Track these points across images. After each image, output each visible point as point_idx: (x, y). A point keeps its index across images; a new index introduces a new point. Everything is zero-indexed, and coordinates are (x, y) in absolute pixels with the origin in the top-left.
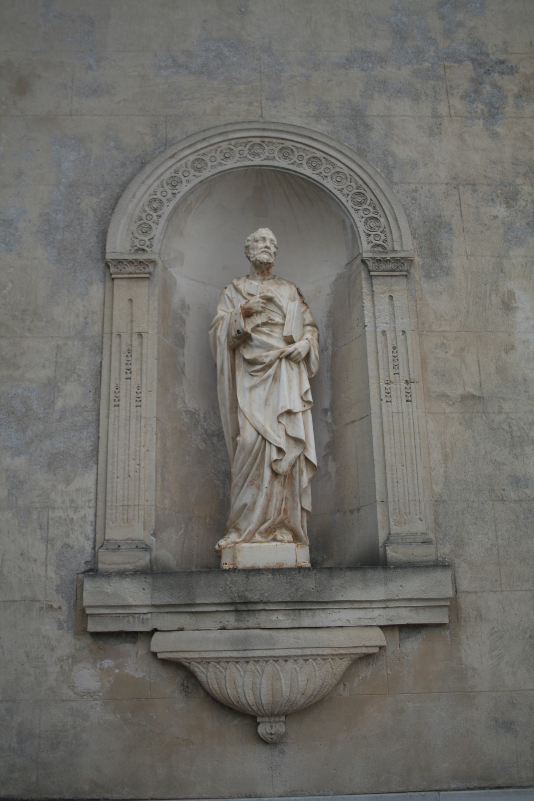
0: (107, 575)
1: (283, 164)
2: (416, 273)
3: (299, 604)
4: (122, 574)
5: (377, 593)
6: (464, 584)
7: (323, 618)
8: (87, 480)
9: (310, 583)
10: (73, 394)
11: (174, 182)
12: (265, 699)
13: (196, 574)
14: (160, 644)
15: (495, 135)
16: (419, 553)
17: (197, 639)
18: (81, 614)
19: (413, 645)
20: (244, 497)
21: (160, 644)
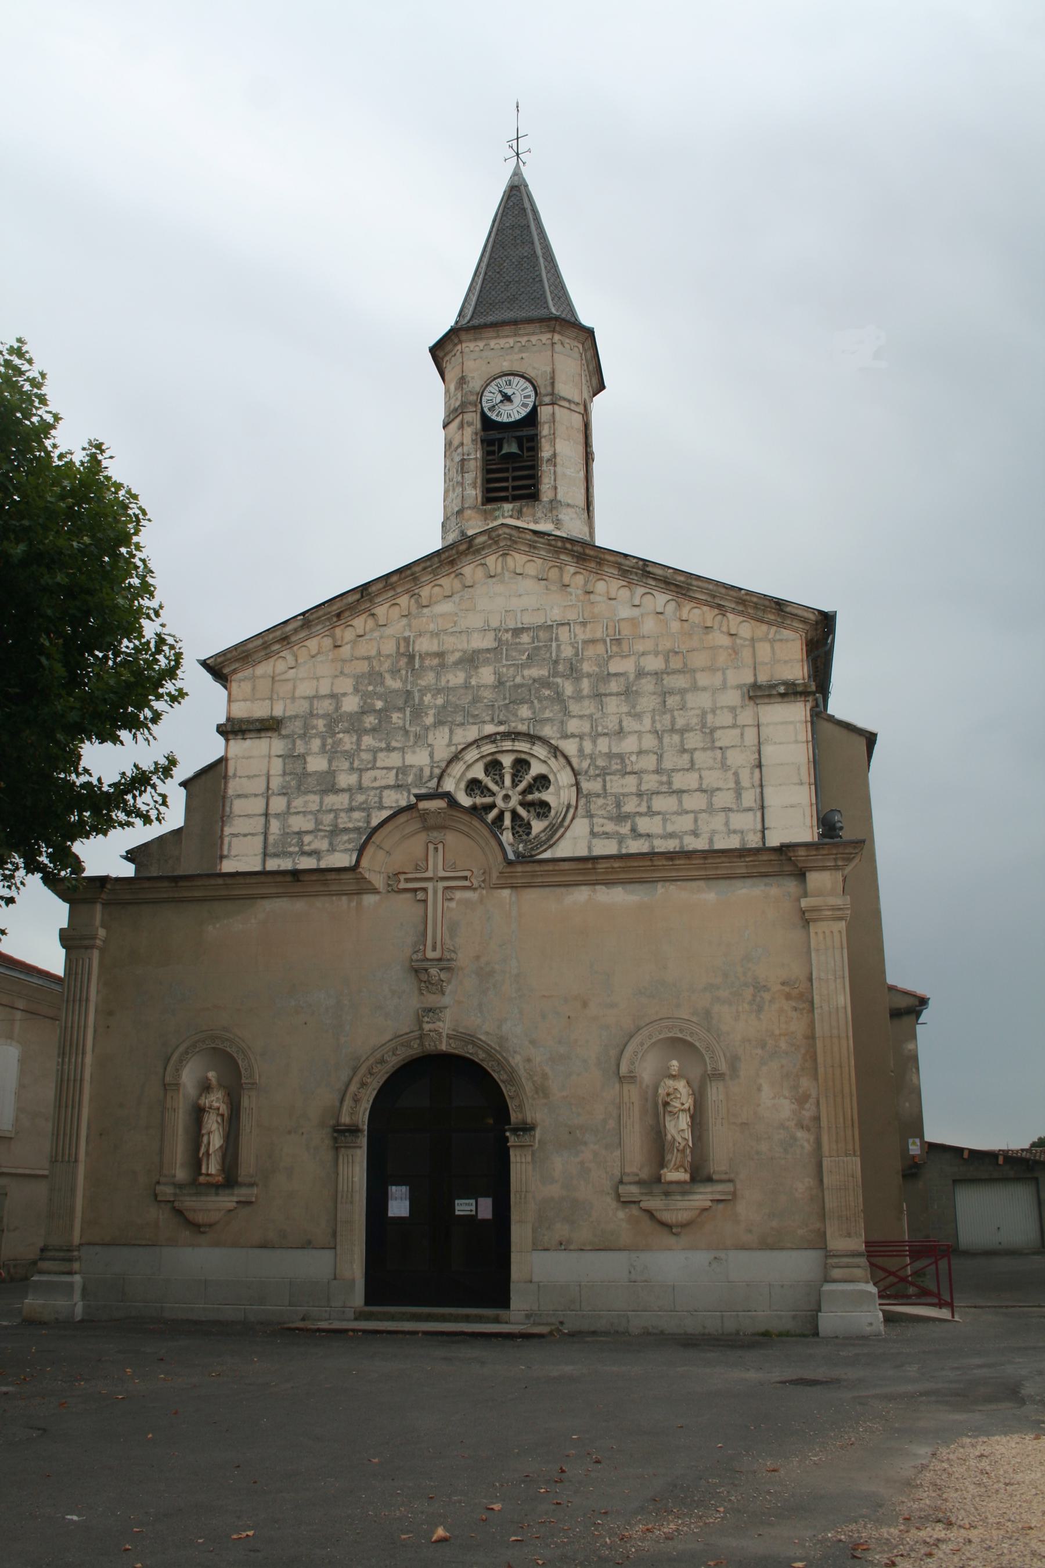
0: (626, 1184)
1: (680, 1036)
2: (727, 1078)
3: (684, 1193)
4: (630, 1183)
5: (709, 1189)
6: (738, 1187)
7: (691, 1197)
8: (617, 1153)
9: (687, 1187)
10: (612, 1124)
11: (642, 1044)
12: (201, 1221)
13: (654, 1182)
14: (643, 1205)
15: (759, 1019)
16: (724, 1177)
17: (653, 1203)
18: (618, 1196)
19: (721, 1206)
20: (668, 1157)
21: (643, 1205)
